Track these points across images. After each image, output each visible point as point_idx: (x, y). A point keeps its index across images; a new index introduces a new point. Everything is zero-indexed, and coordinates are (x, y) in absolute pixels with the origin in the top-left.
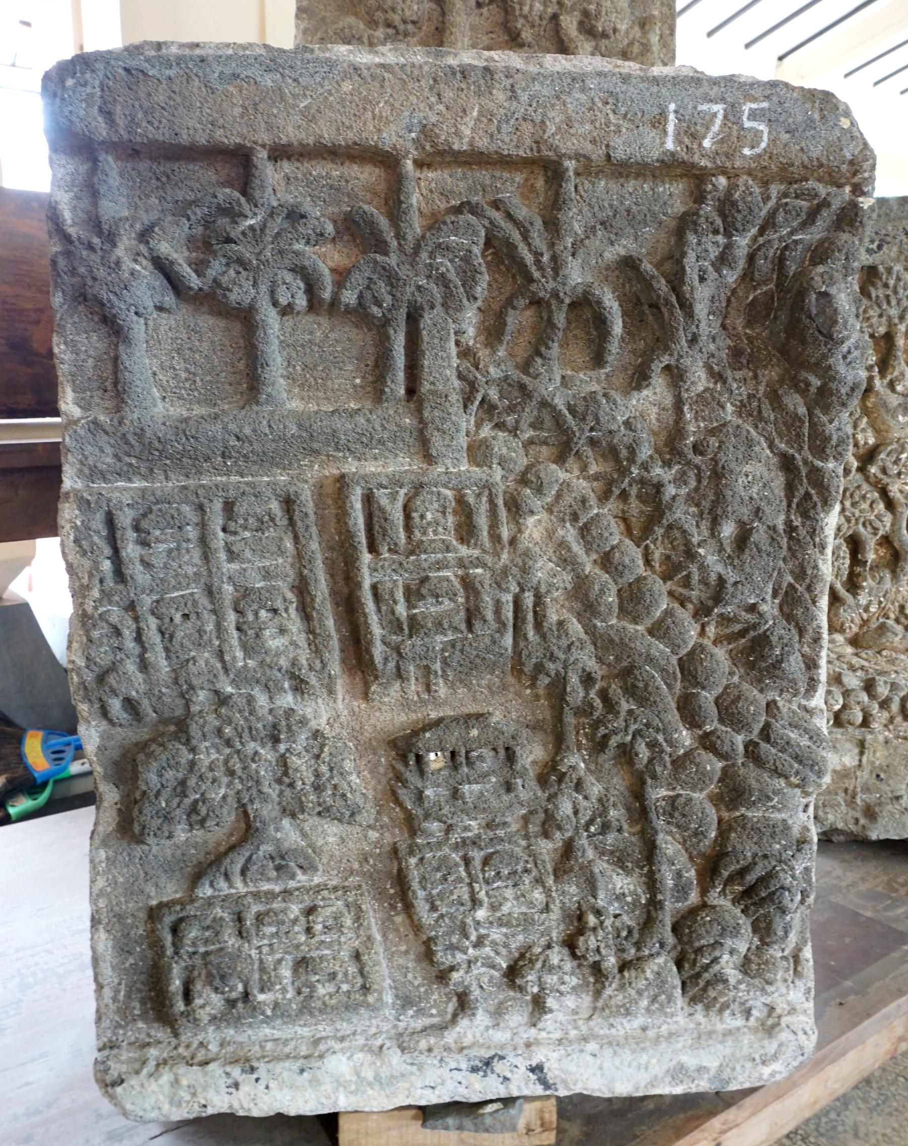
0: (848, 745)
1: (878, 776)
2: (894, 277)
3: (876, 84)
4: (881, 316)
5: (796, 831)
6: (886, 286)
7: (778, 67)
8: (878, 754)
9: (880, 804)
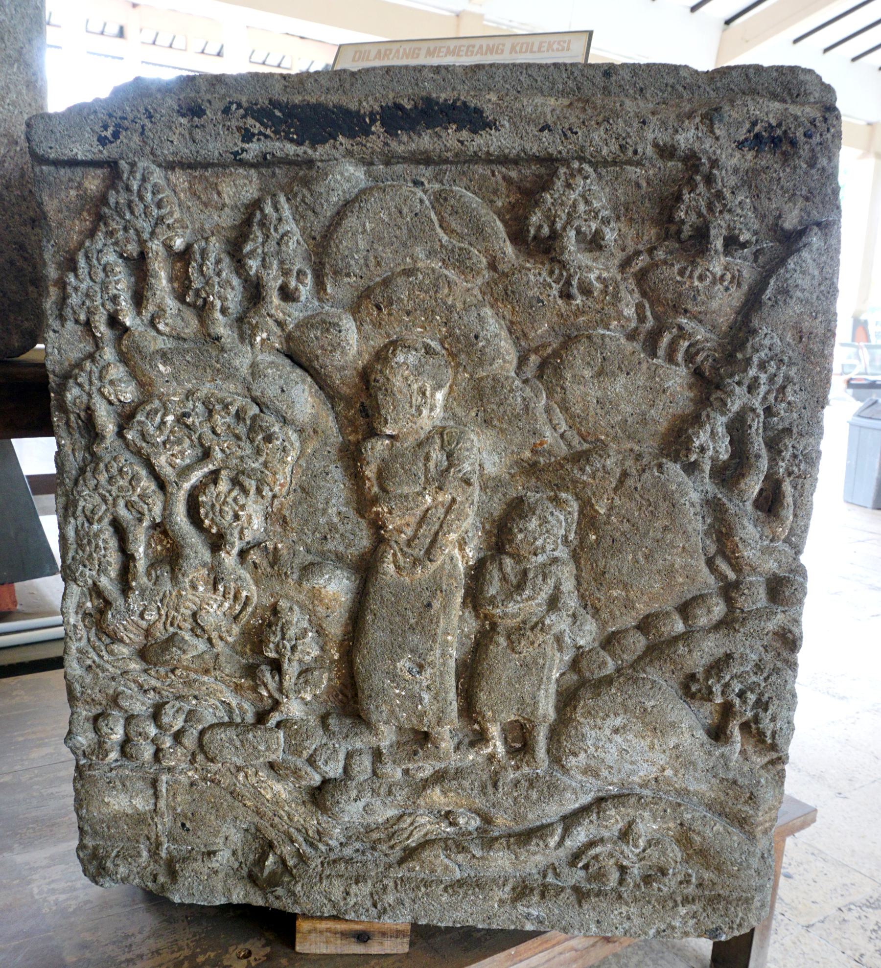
0: (140, 784)
1: (183, 825)
2: (138, 176)
3: (826, 50)
4: (126, 229)
5: (648, 669)
6: (128, 189)
7: (724, 30)
8: (179, 799)
9: (184, 860)
